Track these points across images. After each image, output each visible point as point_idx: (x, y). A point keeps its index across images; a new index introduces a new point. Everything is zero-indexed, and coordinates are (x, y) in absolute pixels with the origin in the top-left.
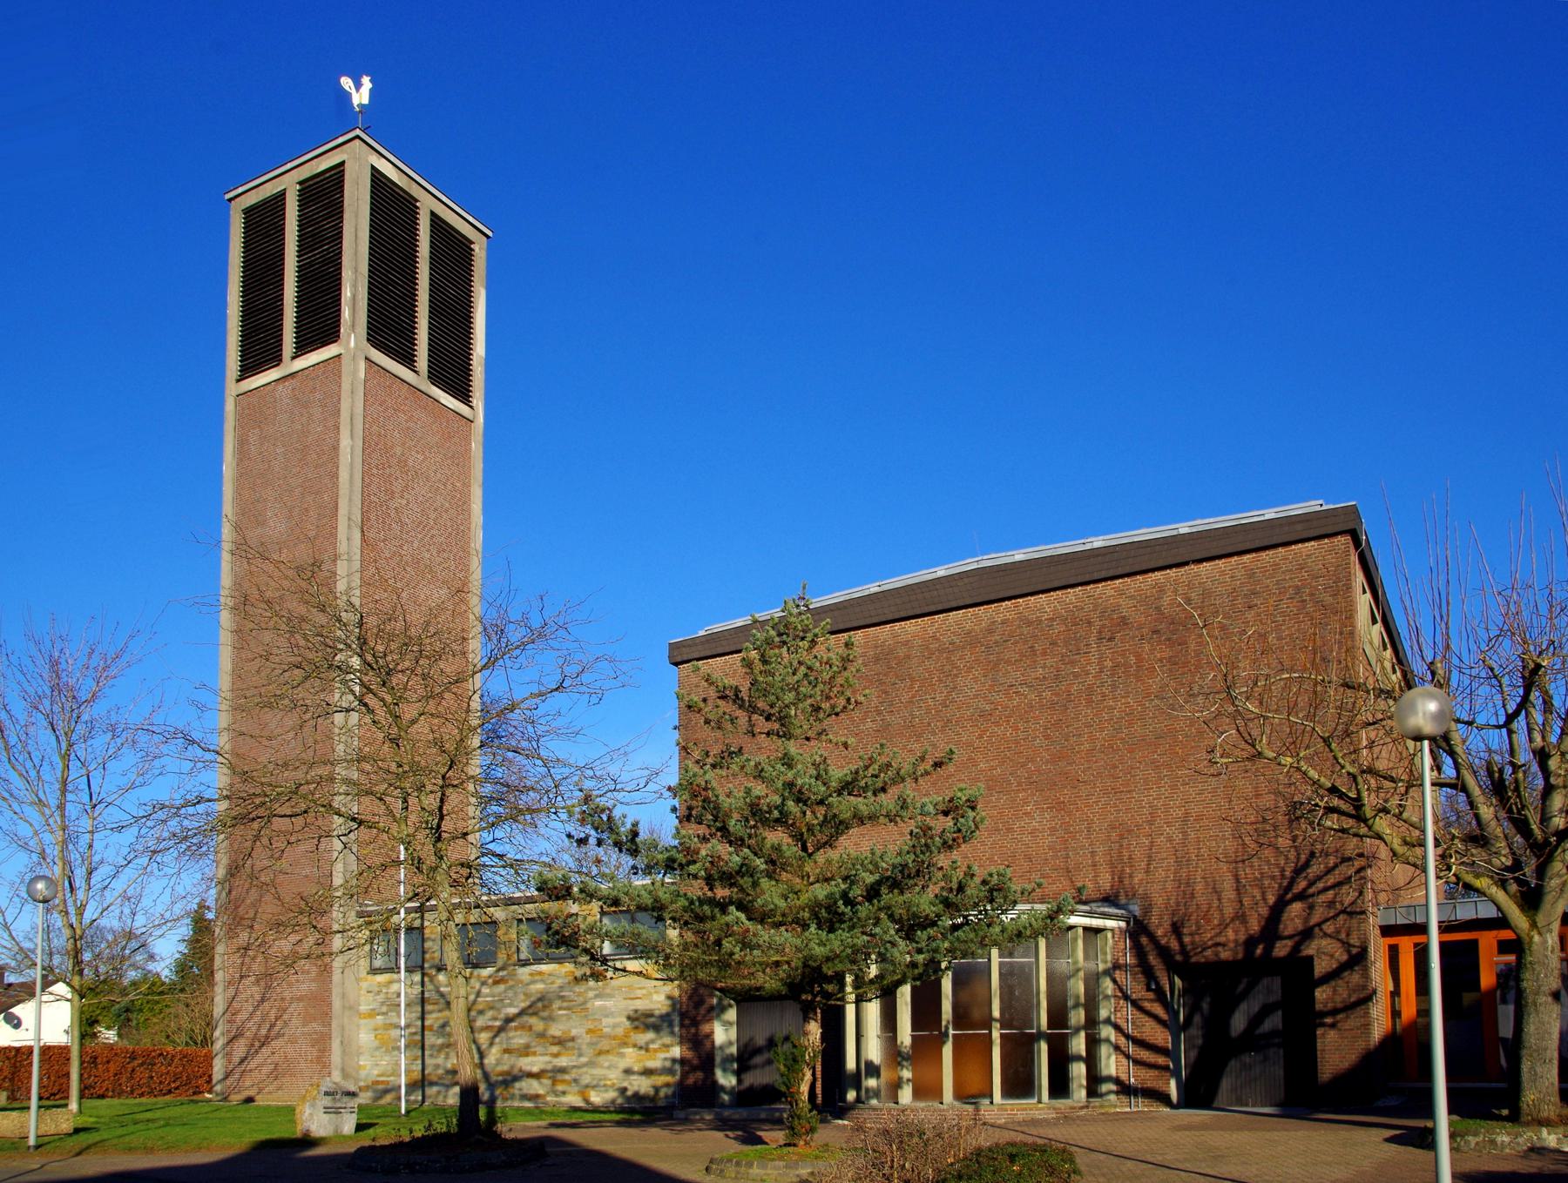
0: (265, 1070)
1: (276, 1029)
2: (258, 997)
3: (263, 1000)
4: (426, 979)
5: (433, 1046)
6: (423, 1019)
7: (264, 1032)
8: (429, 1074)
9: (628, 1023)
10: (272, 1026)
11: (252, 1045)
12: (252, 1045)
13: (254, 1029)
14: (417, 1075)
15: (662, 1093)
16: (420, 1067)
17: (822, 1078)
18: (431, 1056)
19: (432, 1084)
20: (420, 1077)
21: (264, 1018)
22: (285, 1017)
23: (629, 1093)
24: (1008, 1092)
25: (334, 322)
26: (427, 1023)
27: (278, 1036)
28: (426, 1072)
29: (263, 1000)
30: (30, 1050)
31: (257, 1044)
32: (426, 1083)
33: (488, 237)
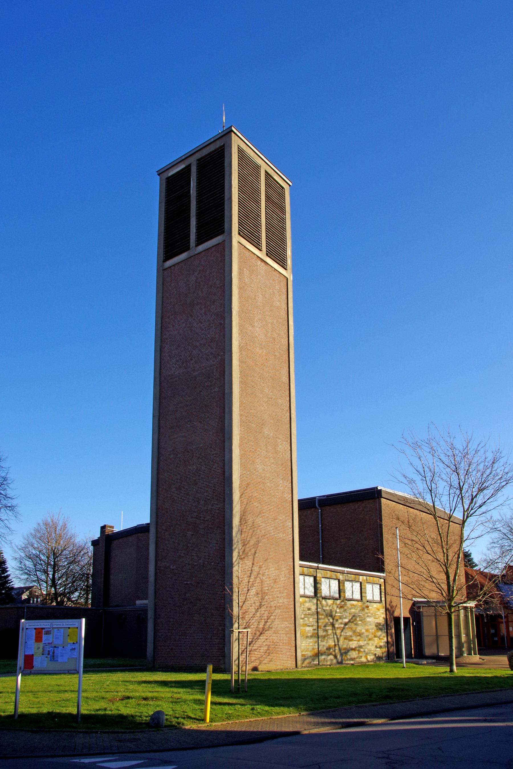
0: (263, 649)
1: (268, 624)
2: (258, 604)
3: (261, 606)
4: (319, 602)
5: (322, 636)
6: (318, 622)
7: (261, 626)
8: (321, 650)
9: (375, 628)
10: (266, 622)
11: (255, 634)
12: (255, 634)
13: (256, 624)
14: (316, 651)
15: (322, 651)
16: (317, 647)
17: (414, 649)
18: (321, 641)
19: (322, 655)
20: (317, 651)
21: (261, 617)
22: (272, 617)
23: (377, 656)
24: (474, 654)
25: (221, 153)
26: (320, 624)
27: (270, 628)
28: (320, 649)
29: (261, 606)
30: (85, 672)
31: (258, 633)
32: (320, 654)
33: (290, 185)
